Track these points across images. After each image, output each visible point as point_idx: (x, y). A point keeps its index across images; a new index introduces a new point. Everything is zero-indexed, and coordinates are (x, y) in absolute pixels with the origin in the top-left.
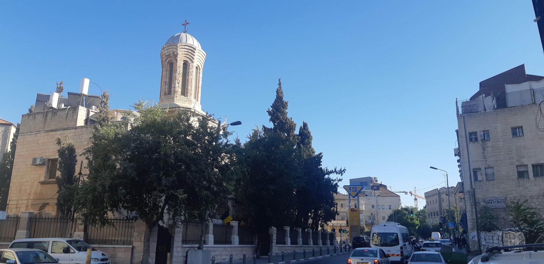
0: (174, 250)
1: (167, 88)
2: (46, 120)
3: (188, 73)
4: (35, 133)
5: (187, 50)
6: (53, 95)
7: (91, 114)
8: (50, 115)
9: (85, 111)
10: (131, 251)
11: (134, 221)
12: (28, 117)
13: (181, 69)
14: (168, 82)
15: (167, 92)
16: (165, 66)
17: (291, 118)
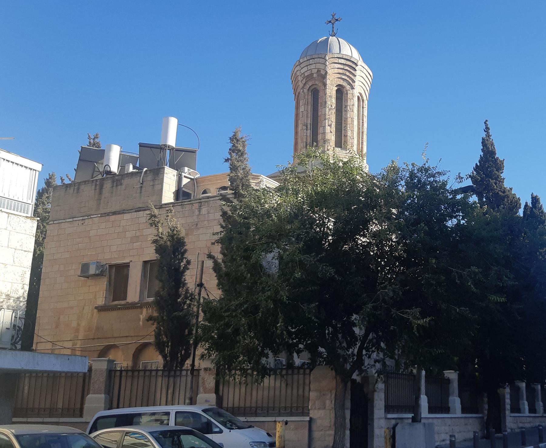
0: (375, 424)
1: (308, 135)
2: (101, 193)
3: (346, 106)
4: (81, 218)
5: (342, 67)
6: (110, 150)
7: (185, 181)
8: (108, 185)
9: (174, 175)
10: (307, 428)
11: (308, 371)
12: (66, 190)
13: (334, 101)
14: (311, 124)
15: (310, 143)
16: (304, 96)
17: (511, 189)
